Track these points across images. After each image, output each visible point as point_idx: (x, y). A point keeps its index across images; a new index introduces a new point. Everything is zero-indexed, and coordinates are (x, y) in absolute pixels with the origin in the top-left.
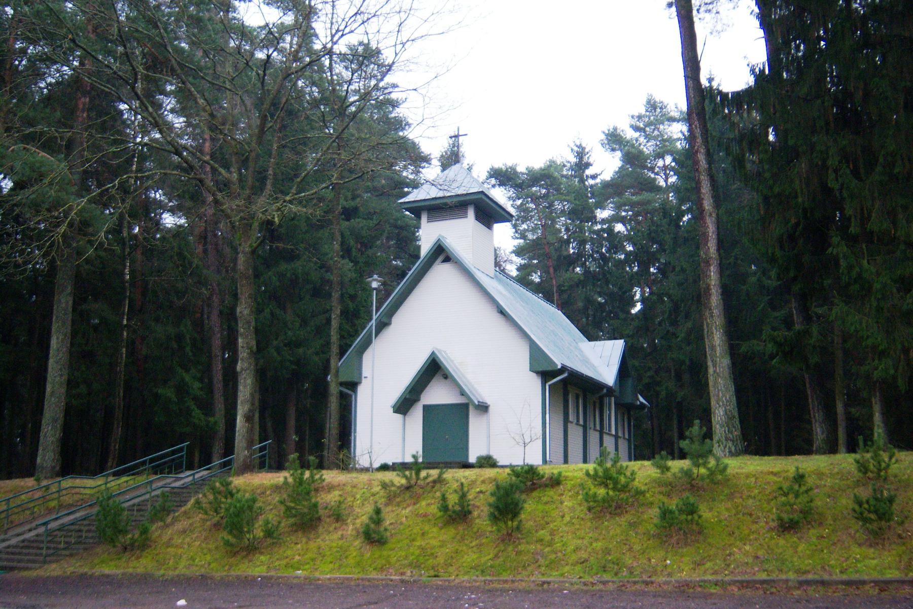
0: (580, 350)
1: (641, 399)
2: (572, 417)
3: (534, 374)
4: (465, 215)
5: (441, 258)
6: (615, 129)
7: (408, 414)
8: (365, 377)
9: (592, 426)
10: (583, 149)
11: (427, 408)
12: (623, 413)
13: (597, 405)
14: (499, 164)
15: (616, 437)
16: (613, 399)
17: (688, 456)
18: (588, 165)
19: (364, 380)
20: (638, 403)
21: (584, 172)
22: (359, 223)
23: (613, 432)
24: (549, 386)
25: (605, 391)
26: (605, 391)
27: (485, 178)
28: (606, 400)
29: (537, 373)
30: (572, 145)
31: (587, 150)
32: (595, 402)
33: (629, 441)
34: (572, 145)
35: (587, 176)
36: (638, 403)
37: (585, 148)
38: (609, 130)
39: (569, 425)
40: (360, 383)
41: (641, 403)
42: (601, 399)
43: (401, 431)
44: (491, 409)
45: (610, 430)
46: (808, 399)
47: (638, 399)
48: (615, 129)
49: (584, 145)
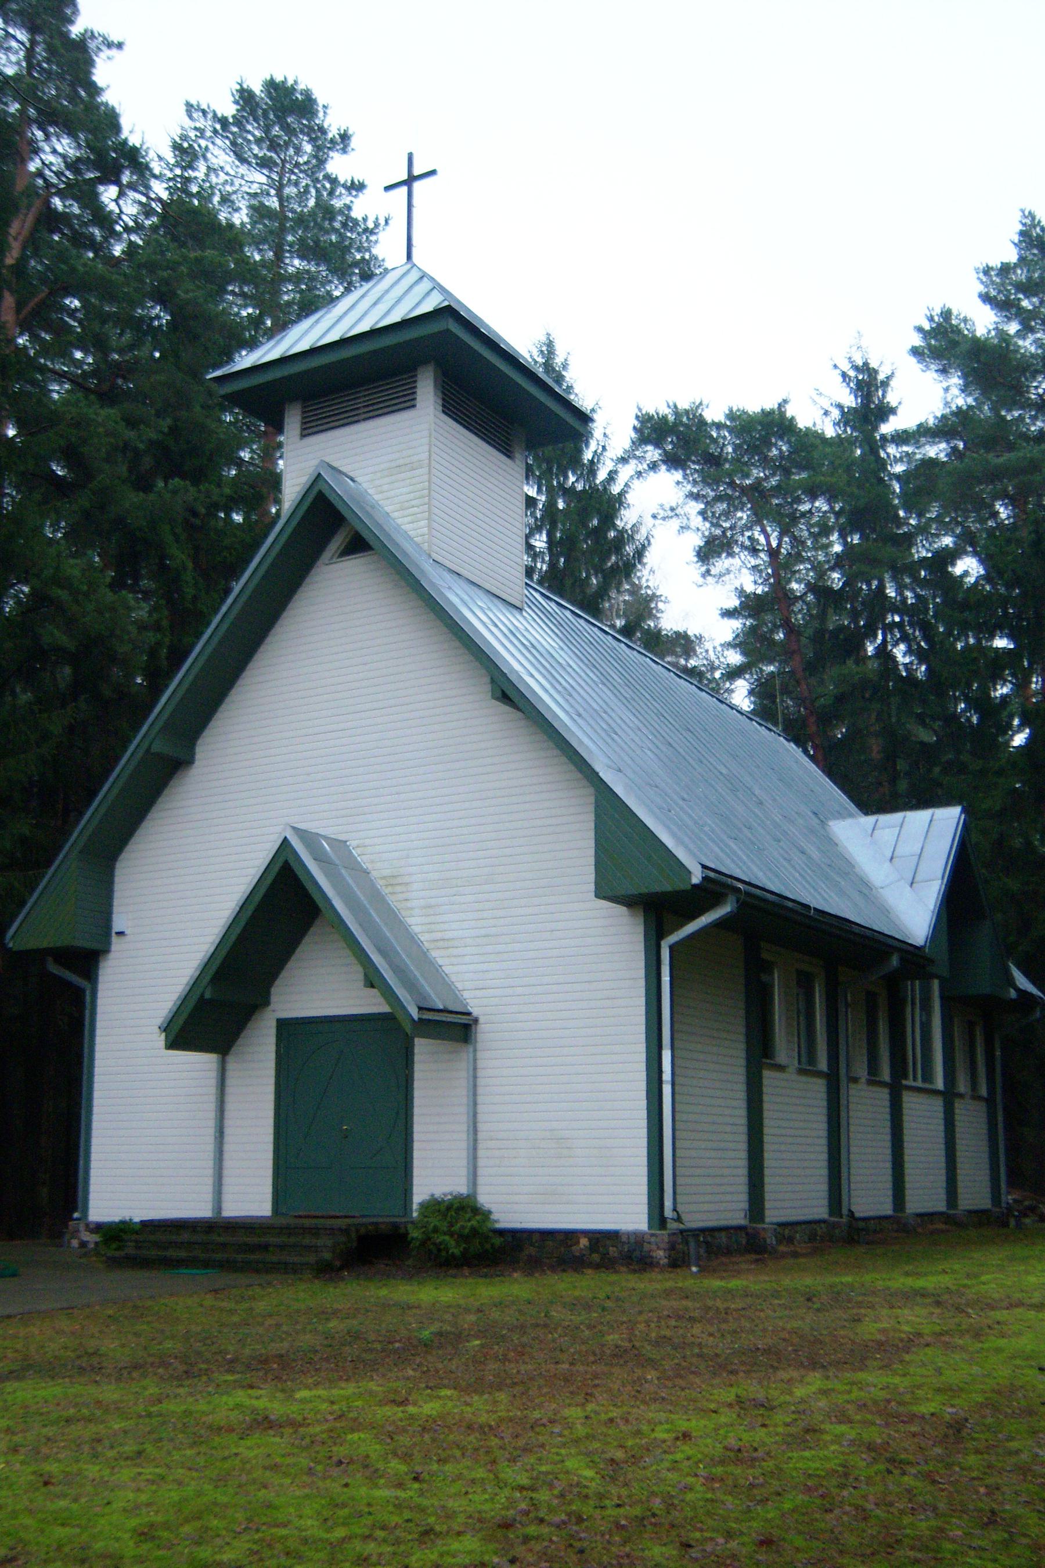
0: (830, 843)
1: (1022, 982)
2: (784, 1049)
3: (622, 910)
4: (406, 402)
5: (337, 543)
6: (947, 314)
7: (234, 1049)
8: (120, 934)
9: (861, 1070)
10: (872, 373)
11: (286, 1028)
12: (971, 1025)
13: (882, 1002)
14: (658, 406)
15: (949, 1096)
16: (936, 983)
17: (964, 347)
18: (885, 412)
19: (116, 944)
20: (1013, 994)
21: (876, 428)
22: (175, 492)
23: (939, 1084)
24: (672, 948)
25: (895, 961)
26: (895, 961)
27: (627, 444)
28: (914, 988)
29: (629, 902)
30: (846, 367)
31: (881, 377)
32: (871, 998)
33: (990, 1101)
34: (846, 367)
35: (883, 437)
36: (1013, 994)
37: (876, 372)
38: (931, 319)
39: (769, 1077)
40: (107, 951)
41: (1022, 993)
42: (893, 984)
43: (211, 1106)
44: (484, 1032)
45: (928, 1077)
46: (370, 914)
47: (1011, 982)
48: (947, 314)
49: (873, 364)
